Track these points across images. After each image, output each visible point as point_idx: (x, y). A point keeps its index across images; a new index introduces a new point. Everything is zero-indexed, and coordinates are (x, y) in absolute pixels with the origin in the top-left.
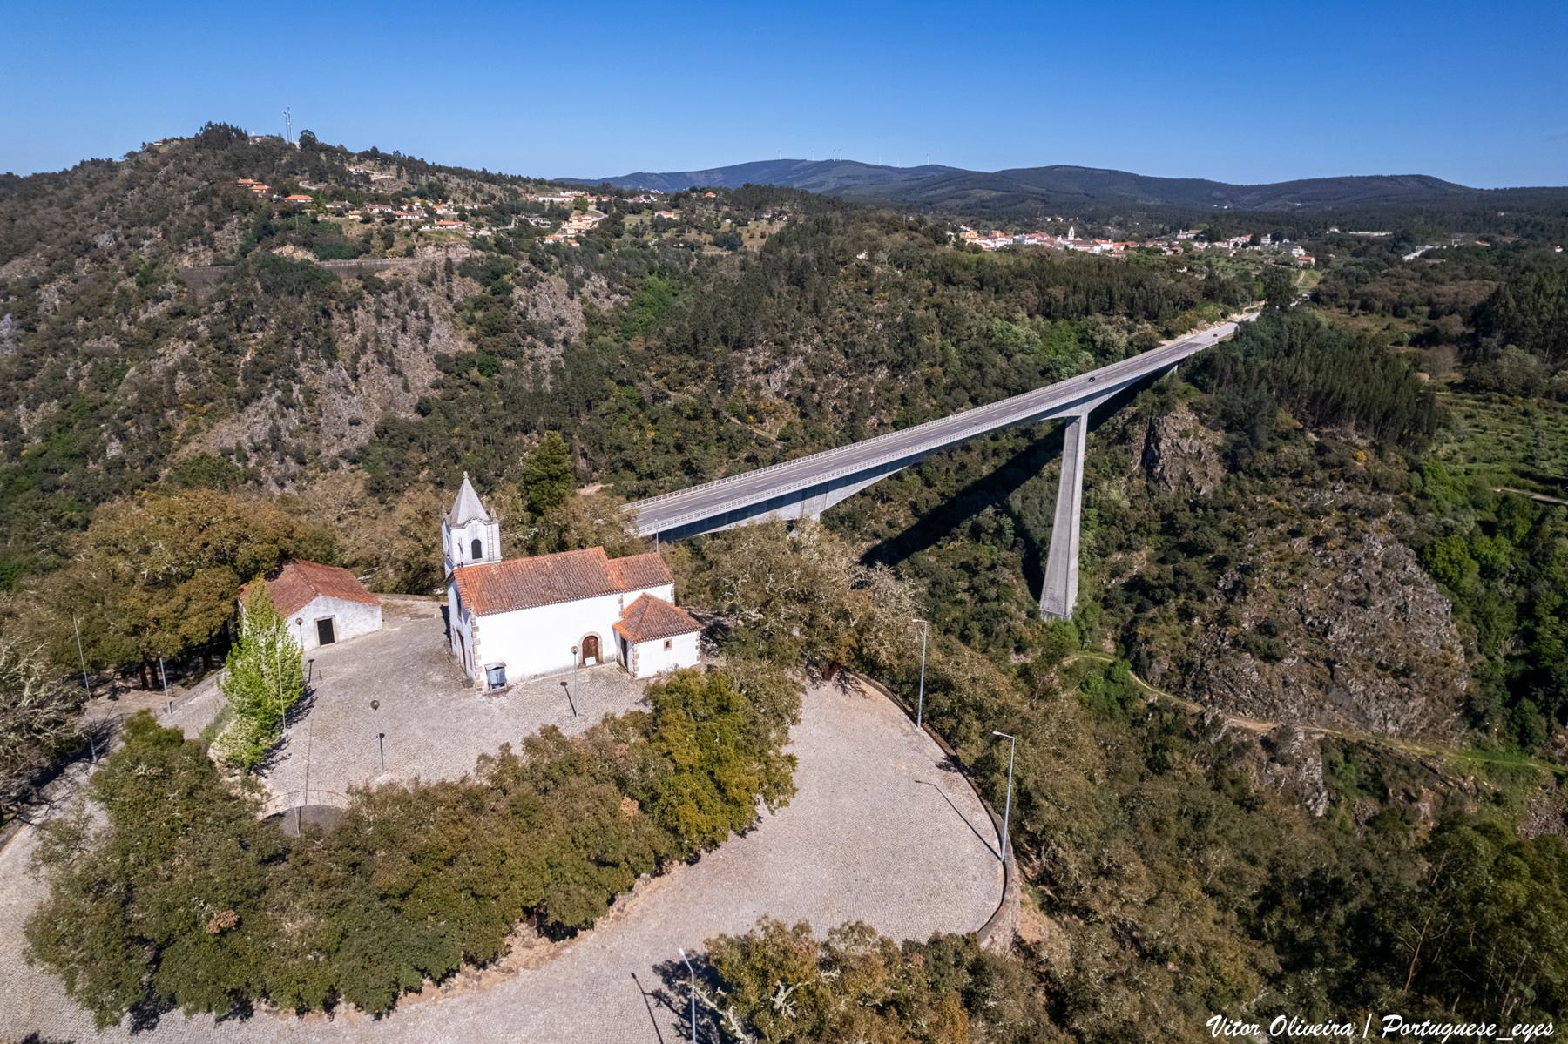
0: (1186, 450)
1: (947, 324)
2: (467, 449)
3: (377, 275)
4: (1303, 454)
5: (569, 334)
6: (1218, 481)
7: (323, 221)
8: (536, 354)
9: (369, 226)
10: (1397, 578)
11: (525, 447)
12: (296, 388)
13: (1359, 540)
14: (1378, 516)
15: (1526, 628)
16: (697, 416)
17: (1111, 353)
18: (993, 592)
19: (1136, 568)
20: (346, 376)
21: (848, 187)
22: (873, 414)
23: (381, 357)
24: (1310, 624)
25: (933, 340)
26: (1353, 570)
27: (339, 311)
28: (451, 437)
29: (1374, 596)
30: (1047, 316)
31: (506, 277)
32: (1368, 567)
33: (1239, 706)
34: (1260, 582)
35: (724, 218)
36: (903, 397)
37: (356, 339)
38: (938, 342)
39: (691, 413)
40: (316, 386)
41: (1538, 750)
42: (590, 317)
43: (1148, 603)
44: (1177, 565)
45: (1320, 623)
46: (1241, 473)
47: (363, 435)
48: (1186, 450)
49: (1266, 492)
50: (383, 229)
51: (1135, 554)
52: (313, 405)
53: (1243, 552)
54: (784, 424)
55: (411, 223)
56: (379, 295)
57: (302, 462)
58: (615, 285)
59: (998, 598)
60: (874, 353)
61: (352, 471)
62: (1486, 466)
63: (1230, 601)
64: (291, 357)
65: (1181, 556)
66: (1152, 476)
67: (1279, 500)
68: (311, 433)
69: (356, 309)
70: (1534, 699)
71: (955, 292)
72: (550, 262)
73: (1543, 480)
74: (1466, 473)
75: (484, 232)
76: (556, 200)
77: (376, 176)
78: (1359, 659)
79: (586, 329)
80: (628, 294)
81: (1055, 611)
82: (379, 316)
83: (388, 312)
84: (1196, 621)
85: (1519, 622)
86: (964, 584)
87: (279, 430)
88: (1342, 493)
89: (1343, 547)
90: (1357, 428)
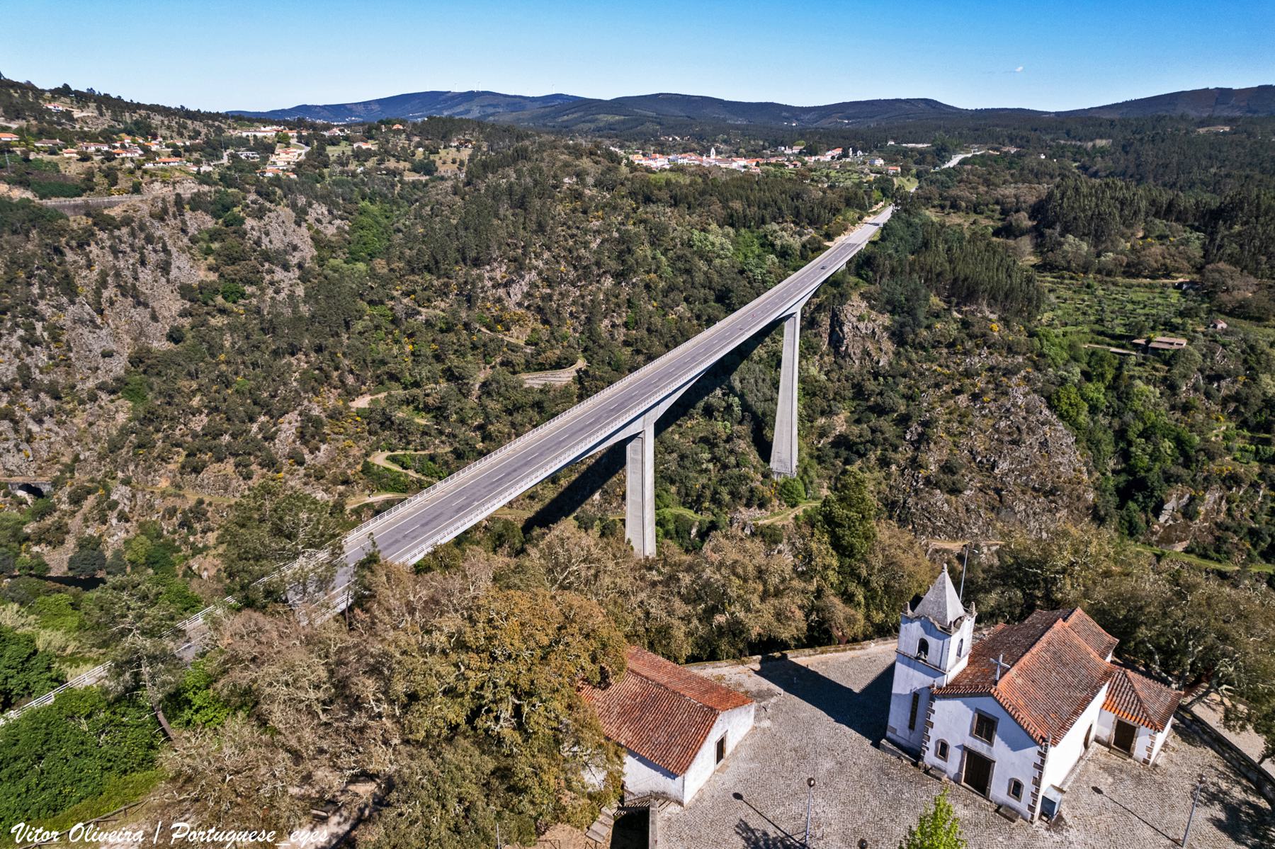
0: (864, 331)
1: (655, 236)
2: (236, 374)
3: (106, 212)
4: (953, 329)
5: (304, 258)
6: (891, 354)
7: (36, 160)
8: (276, 279)
9: (88, 164)
10: (1038, 421)
11: (294, 368)
12: (39, 325)
13: (1005, 393)
14: (1016, 374)
15: (1122, 448)
16: (449, 329)
17: (789, 255)
18: (732, 460)
19: (838, 429)
20: (91, 311)
21: (493, 114)
22: (605, 317)
23: (124, 290)
24: (980, 462)
25: (644, 251)
26: (1006, 417)
27: (71, 248)
28: (217, 364)
29: (1024, 436)
30: (732, 225)
31: (236, 210)
32: (1016, 414)
33: (936, 532)
34: (938, 432)
35: (417, 147)
36: (629, 301)
37: (94, 275)
38: (649, 253)
39: (444, 326)
40: (61, 322)
41: (1142, 538)
42: (318, 241)
43: (854, 457)
44: (871, 424)
45: (988, 460)
46: (908, 347)
47: (118, 366)
48: (864, 331)
49: (929, 360)
50: (104, 167)
51: (835, 418)
52: (60, 341)
53: (920, 410)
54: (529, 331)
55: (132, 160)
56: (111, 231)
57: (57, 397)
58: (335, 212)
59: (738, 465)
60: (598, 264)
61: (112, 401)
62: (1074, 329)
63: (917, 449)
64: (29, 295)
65: (873, 417)
66: (839, 353)
67: (940, 366)
68: (63, 369)
69: (89, 245)
70: (1136, 501)
71: (655, 209)
72: (275, 193)
73: (1113, 337)
74: (1064, 335)
75: (205, 168)
76: (259, 135)
77: (77, 114)
78: (1018, 485)
79: (316, 253)
80: (347, 219)
81: (783, 470)
82: (115, 252)
83: (123, 247)
84: (894, 467)
85: (1117, 444)
86: (707, 456)
87: (29, 368)
88: (987, 357)
89: (995, 400)
90: (989, 305)
